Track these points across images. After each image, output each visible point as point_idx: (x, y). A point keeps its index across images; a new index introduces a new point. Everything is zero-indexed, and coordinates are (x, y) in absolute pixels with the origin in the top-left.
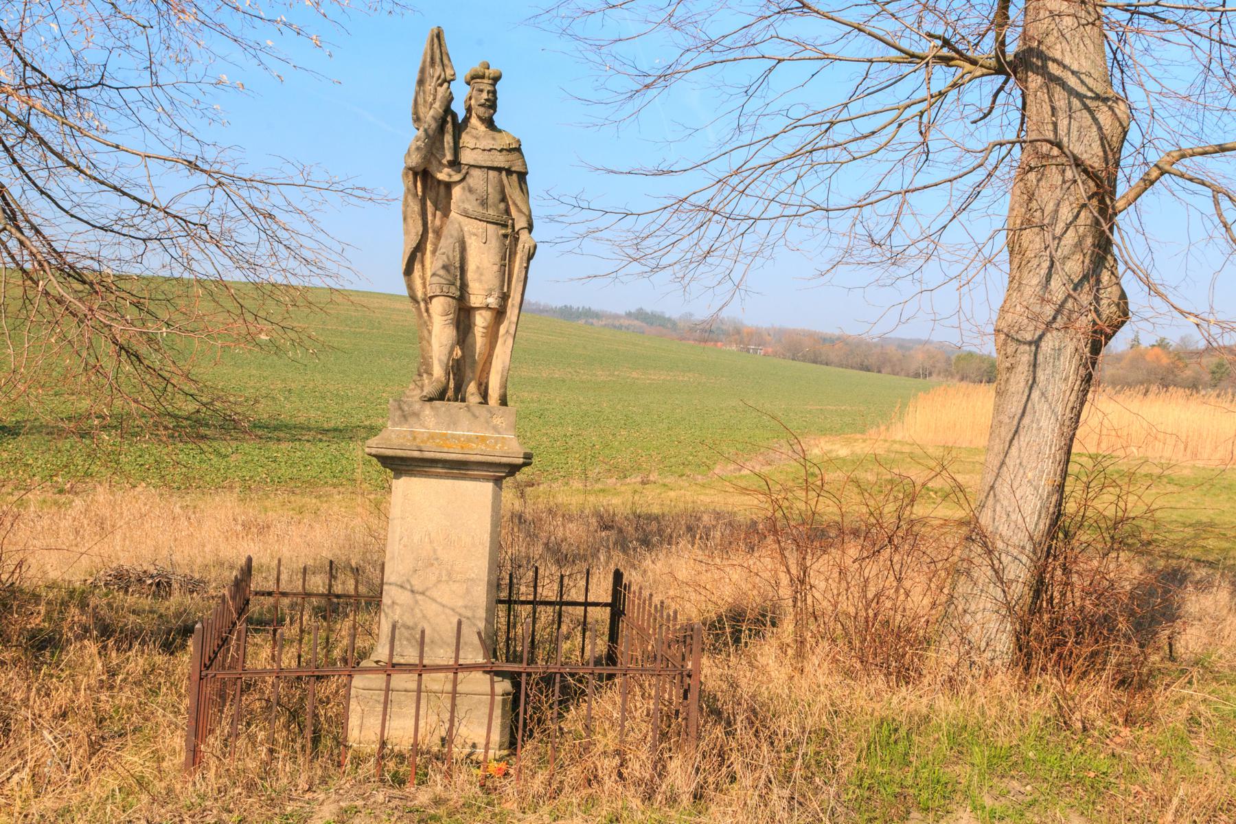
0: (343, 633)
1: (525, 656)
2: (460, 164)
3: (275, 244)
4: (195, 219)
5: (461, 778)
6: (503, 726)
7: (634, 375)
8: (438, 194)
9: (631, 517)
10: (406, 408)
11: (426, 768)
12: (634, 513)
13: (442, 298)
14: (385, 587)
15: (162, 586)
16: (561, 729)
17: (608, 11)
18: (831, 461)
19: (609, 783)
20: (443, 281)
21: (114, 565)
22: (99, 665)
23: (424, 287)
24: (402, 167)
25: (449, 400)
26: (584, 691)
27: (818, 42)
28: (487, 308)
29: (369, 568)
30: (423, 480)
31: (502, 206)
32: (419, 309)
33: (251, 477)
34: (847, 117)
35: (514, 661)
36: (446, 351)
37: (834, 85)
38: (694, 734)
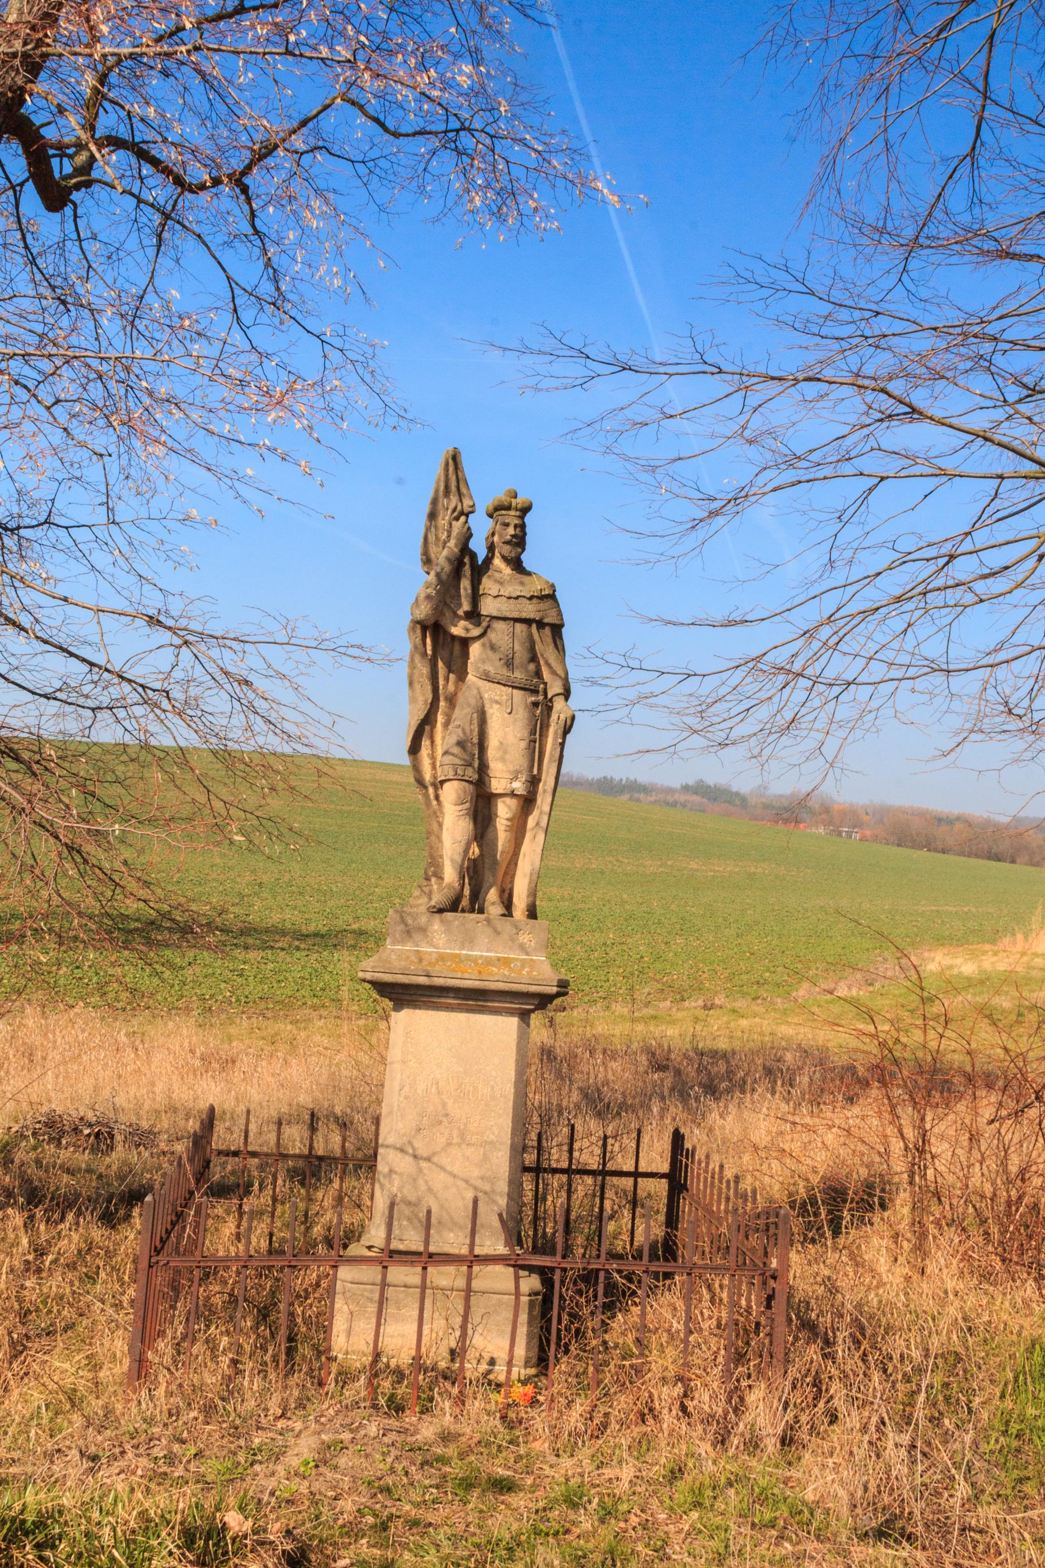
0: (325, 1203)
1: (559, 1247)
2: (479, 615)
3: (252, 716)
4: (157, 685)
5: (474, 1406)
6: (530, 1336)
7: (693, 865)
8: (452, 653)
9: (691, 1054)
10: (410, 922)
11: (431, 1389)
12: (695, 1050)
13: (455, 783)
14: (381, 1150)
15: (102, 1138)
16: (605, 1343)
17: (663, 423)
18: (955, 985)
19: (669, 1418)
20: (457, 761)
21: (44, 1109)
22: (25, 1241)
23: (434, 767)
24: (406, 620)
25: (463, 911)
26: (634, 1293)
27: (931, 454)
28: (513, 794)
29: (357, 1117)
30: (431, 1013)
31: (532, 667)
32: (426, 796)
33: (212, 996)
34: (971, 548)
35: (544, 1253)
36: (460, 849)
37: (953, 509)
38: (781, 1356)
